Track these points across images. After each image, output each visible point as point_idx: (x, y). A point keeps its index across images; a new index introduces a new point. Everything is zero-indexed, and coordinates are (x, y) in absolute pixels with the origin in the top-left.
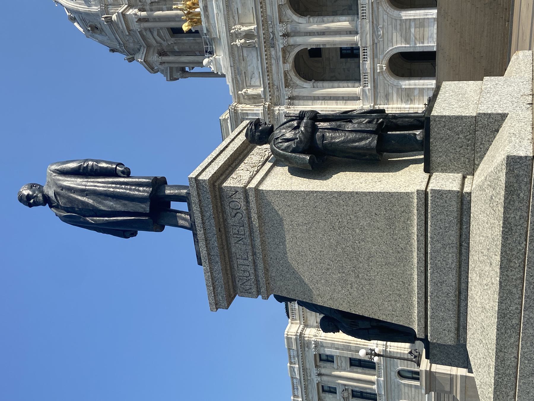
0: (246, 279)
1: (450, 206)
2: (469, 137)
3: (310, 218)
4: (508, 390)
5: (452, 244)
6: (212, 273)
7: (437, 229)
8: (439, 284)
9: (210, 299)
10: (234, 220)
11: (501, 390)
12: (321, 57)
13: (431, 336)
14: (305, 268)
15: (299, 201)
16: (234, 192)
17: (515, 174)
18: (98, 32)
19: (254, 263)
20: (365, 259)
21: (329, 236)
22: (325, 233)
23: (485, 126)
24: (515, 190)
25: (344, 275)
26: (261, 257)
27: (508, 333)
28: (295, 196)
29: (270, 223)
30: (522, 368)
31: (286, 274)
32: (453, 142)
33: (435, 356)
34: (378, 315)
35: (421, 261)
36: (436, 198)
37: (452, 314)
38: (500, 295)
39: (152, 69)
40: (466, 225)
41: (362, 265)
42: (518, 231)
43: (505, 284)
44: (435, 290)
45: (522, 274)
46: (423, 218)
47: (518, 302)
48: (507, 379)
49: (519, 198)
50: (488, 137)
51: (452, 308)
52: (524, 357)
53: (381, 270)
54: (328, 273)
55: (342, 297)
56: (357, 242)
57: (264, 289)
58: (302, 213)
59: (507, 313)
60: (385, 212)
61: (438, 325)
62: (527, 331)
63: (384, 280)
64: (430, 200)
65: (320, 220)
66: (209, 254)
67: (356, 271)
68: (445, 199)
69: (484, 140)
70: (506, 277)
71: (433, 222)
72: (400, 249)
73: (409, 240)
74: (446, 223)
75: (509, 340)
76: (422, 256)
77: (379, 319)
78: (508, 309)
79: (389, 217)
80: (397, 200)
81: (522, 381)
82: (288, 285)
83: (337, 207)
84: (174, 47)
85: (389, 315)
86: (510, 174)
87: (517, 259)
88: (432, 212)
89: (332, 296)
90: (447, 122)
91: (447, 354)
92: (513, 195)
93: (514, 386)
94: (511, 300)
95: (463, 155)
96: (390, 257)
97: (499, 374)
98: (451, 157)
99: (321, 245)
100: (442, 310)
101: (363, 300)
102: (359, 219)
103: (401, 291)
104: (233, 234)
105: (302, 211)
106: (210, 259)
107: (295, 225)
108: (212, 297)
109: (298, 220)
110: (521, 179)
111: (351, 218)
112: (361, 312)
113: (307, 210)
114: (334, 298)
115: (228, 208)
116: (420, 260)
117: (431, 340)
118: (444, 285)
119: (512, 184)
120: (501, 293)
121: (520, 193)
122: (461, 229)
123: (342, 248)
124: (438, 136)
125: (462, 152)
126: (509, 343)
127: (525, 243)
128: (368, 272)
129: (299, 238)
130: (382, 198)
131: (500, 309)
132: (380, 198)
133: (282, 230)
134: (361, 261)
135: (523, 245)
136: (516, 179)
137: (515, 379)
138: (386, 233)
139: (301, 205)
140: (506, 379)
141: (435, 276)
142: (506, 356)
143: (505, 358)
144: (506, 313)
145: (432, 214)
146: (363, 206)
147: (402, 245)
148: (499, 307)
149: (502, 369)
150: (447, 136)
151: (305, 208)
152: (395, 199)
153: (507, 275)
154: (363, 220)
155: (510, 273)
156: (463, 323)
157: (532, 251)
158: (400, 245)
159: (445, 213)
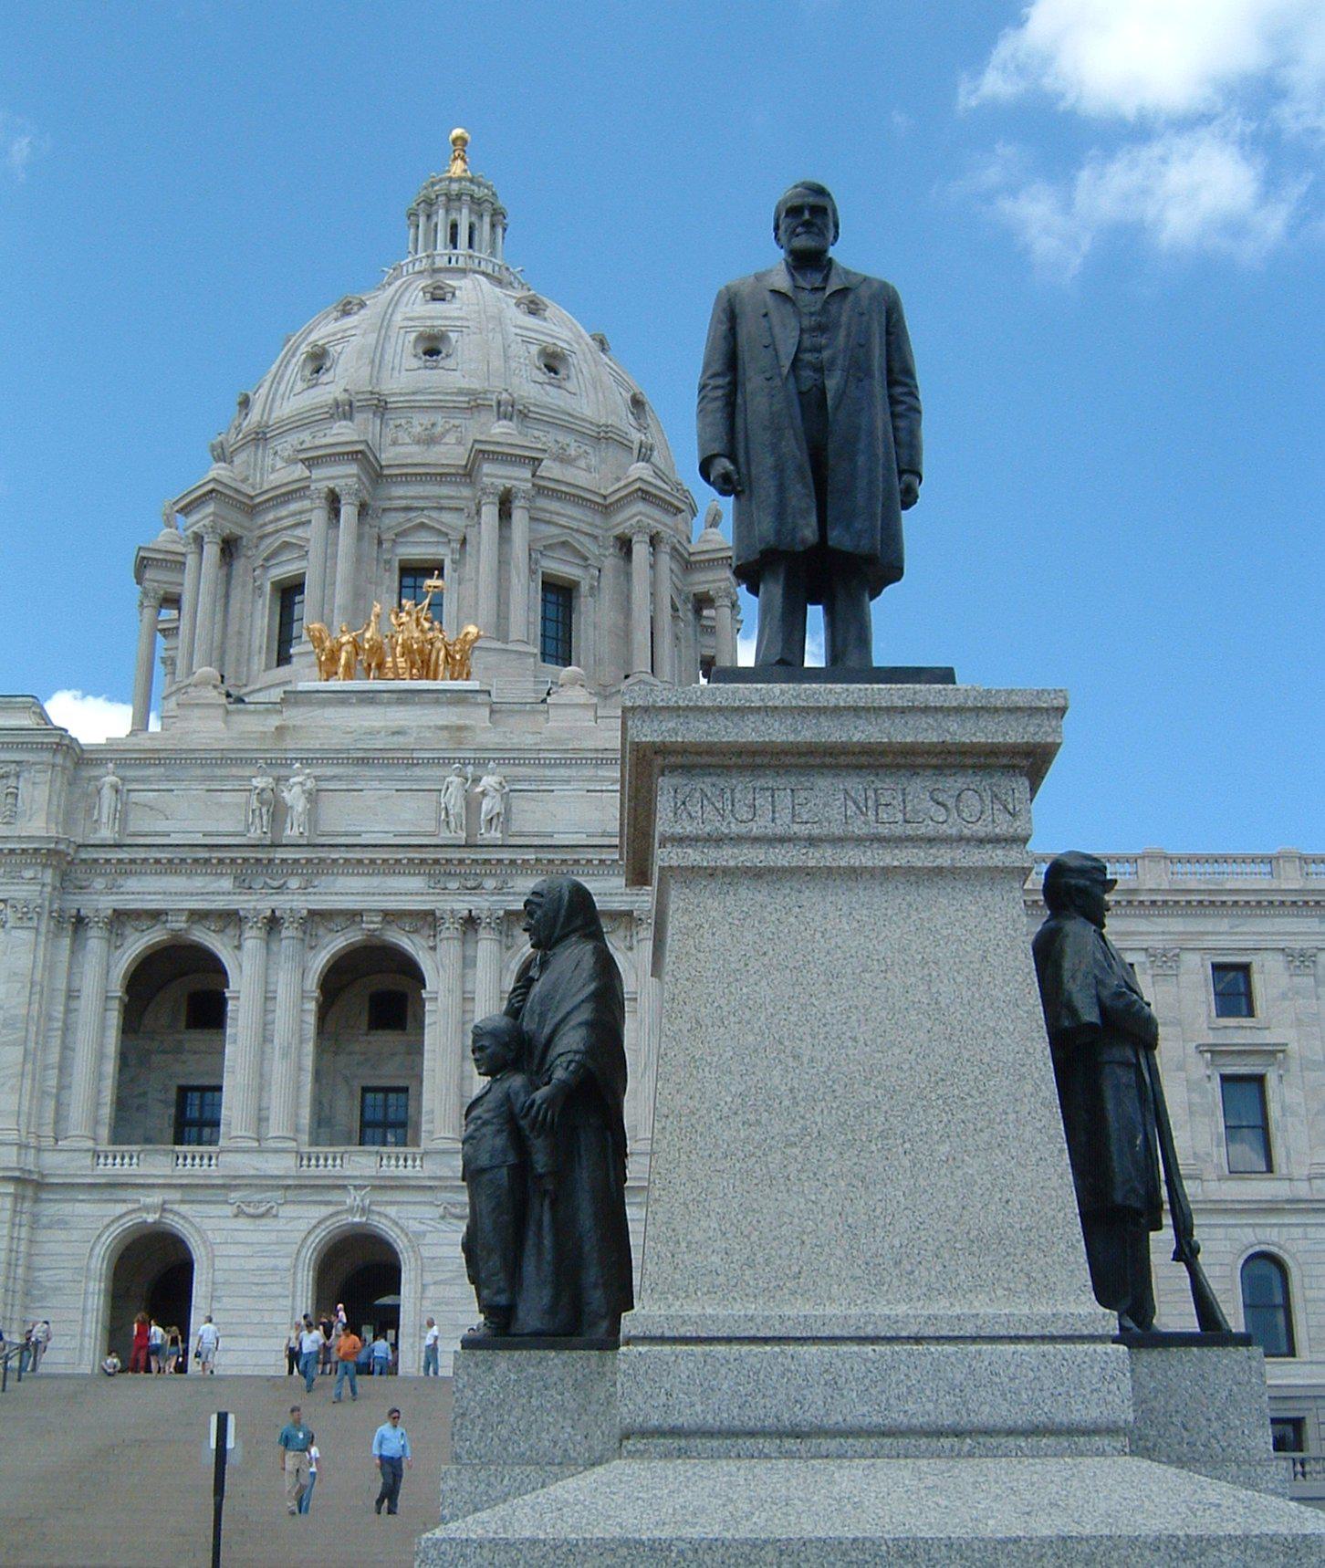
5: (968, 1409)
10: (922, 797)
12: (189, 1026)
13: (640, 1353)
16: (1010, 807)
18: (307, 373)
19: (782, 840)
20: (856, 1167)
21: (911, 1068)
22: (918, 1056)
25: (786, 1103)
31: (755, 931)
32: (1195, 1405)
35: (894, 1326)
36: (1103, 1365)
37: (729, 1416)
41: (833, 1157)
43: (1015, 1554)
44: (806, 1366)
51: (752, 1415)
54: (782, 1056)
56: (907, 1145)
58: (970, 993)
59: (917, 1563)
65: (957, 1045)
67: (808, 1138)
70: (1035, 1555)
71: (1027, 1359)
74: (1030, 1393)
76: (912, 1330)
79: (1003, 1236)
82: (713, 934)
83: (1008, 1095)
88: (1059, 1357)
90: (1248, 1388)
92: (1286, 1555)
95: (1162, 1432)
98: (1155, 1404)
99: (873, 1041)
100: (741, 1388)
101: (710, 1156)
102: (982, 1154)
103: (767, 1269)
104: (876, 790)
107: (926, 971)
109: (946, 981)
113: (983, 1010)
116: (896, 1322)
117: (624, 1354)
118: (830, 1391)
122: (1011, 1432)
128: (812, 1176)
132: (1061, 1215)
134: (846, 1156)
138: (954, 1228)
139: (993, 992)
141: (856, 1367)
145: (1055, 1356)
146: (1025, 1167)
147: (925, 1273)
148: (936, 1541)
149: (718, 1558)
150: (1212, 1391)
152: (1066, 1255)
153: (1042, 1556)
154: (983, 1167)
159: (1060, 1389)
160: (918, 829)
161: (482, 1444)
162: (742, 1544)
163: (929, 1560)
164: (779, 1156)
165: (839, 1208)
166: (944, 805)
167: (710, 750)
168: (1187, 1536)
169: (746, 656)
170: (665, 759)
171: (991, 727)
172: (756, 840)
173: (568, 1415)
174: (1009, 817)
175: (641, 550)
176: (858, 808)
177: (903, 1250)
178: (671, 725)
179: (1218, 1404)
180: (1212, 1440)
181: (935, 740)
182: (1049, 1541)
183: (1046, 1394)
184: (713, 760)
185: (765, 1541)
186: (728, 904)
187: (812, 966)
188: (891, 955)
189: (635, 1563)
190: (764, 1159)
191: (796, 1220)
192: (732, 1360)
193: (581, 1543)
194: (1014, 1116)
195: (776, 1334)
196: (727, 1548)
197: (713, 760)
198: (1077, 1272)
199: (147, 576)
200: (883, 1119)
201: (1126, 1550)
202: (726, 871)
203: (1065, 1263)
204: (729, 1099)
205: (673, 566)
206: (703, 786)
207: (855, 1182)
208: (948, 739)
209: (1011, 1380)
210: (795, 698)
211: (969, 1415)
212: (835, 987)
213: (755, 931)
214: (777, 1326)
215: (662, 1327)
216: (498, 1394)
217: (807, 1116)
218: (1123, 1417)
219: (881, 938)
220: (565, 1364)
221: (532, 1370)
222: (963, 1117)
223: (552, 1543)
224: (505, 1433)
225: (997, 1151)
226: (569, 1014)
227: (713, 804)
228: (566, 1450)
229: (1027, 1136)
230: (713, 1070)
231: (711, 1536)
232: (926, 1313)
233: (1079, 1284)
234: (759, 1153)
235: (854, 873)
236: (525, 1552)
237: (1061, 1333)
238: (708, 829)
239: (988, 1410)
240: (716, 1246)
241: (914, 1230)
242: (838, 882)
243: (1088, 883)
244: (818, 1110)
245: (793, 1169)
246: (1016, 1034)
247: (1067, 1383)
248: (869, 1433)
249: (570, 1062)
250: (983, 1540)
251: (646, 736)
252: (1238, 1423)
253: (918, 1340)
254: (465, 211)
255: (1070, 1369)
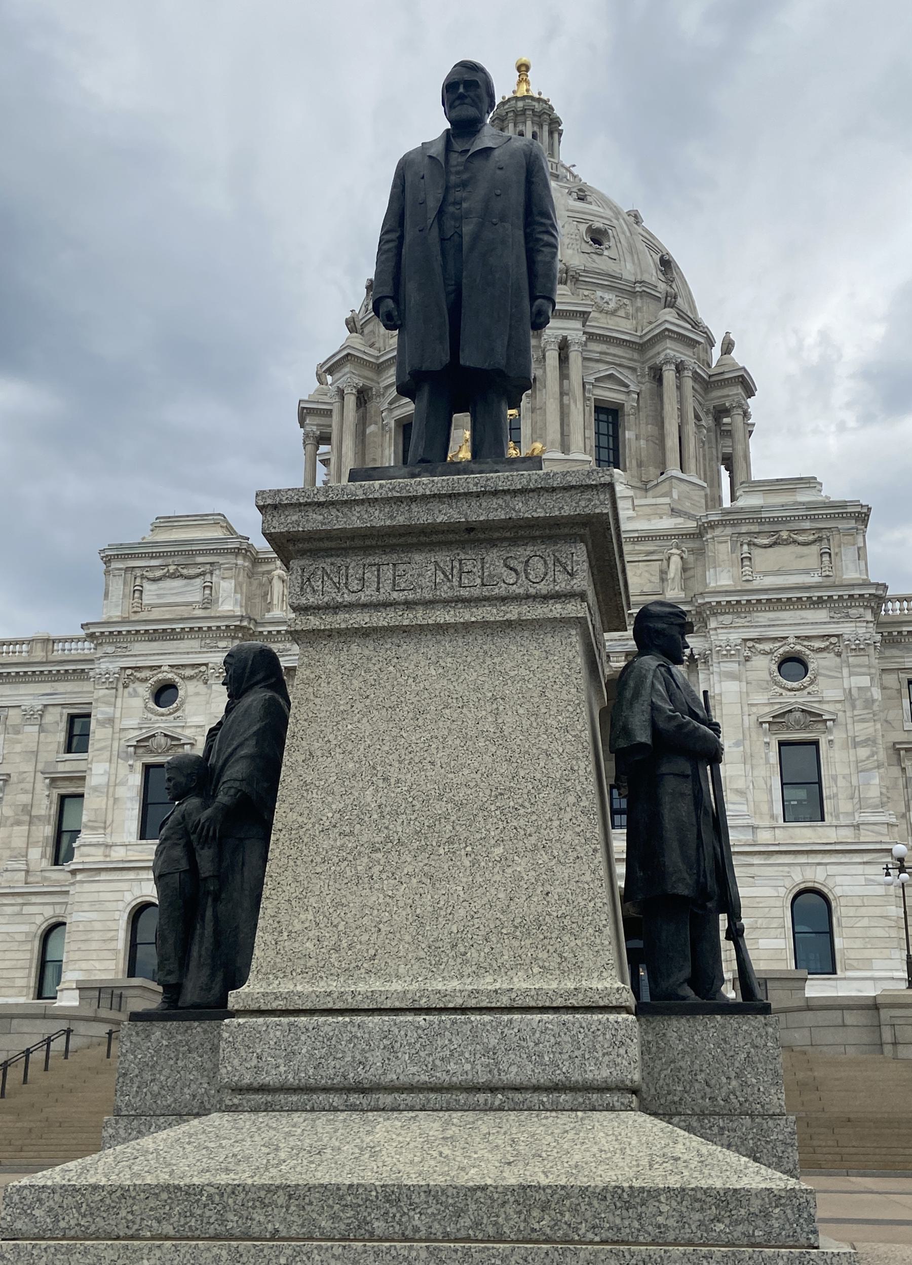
0: (339, 583)
1: (596, 1064)
2: (735, 1101)
3: (518, 740)
4: (175, 1219)
5: (499, 1069)
6: (362, 502)
7: (534, 1034)
8: (385, 1042)
9: (290, 492)
10: (497, 564)
11: (176, 1202)
13: (239, 1025)
14: (383, 727)
15: (560, 718)
16: (569, 568)
17: (770, 1209)
19: (386, 605)
21: (477, 785)
23: (764, 1137)
24: (731, 1211)
25: (375, 816)
26: (406, 623)
27: (342, 1211)
28: (571, 709)
29: (493, 647)
30: (262, 1250)
31: (361, 679)
32: (717, 1065)
33: (143, 1036)
34: (275, 897)
36: (613, 1032)
37: (308, 1075)
38: (451, 1188)
39: (330, 371)
40: (548, 1101)
41: (409, 860)
42: (627, 1223)
43: (482, 1200)
44: (369, 1033)
45: (513, 1236)
46: (559, 1002)
47: (433, 1231)
48: (210, 1217)
49: (712, 1220)
50: (739, 1143)
51: (324, 1074)
52: (295, 1254)
53: (401, 904)
55: (314, 811)
56: (469, 849)
57: (317, 623)
58: (529, 722)
59: (401, 1206)
60: (555, 914)
61: (272, 1043)
62: (372, 1258)
63: (375, 912)
64: (608, 1019)
65: (515, 765)
66: (413, 499)
67: (390, 844)
68: (614, 1053)
69: (732, 1134)
70: (500, 1201)
72: (462, 950)
73: (491, 971)
74: (551, 1056)
75: (323, 1216)
76: (458, 1002)
77: (263, 900)
78: (414, 1210)
79: (543, 923)
80: (589, 942)
81: (224, 1253)
82: (329, 683)
83: (554, 805)
84: (376, 423)
85: (279, 922)
86: (770, 1199)
87: (553, 1223)
88: (577, 1025)
89: (313, 786)
90: (764, 1052)
91: (153, 1066)
93: (189, 1234)
94: (439, 1214)
96: (440, 926)
97: (222, 1195)
98: (681, 1063)
99: (448, 764)
101: (312, 861)
102: (529, 854)
103: (350, 953)
104: (460, 561)
105: (535, 724)
106: (399, 500)
107: (495, 706)
108: (296, 497)
109: (510, 713)
110: (760, 1222)
111: (530, 835)
112: (277, 855)
113: (539, 736)
114: (307, 790)
115: (528, 553)
116: (445, 996)
117: (226, 1025)
118: (387, 1054)
119: (744, 1203)
120: (455, 1190)
121: (723, 1223)
122: (537, 1089)
123: (449, 814)
124: (729, 1033)
125: (697, 1086)
126: (315, 1215)
127: (597, 1239)
128: (390, 875)
129: (462, 713)
130: (590, 909)
131: (409, 1189)
132: (592, 904)
133: (478, 676)
134: (419, 859)
135: (590, 1236)
136: (757, 1212)
137: (212, 1235)
138: (502, 917)
139: (549, 721)
140: (208, 1213)
141: (409, 1034)
142: (275, 1210)
143: (270, 1208)
144: (402, 1204)
145: (573, 1024)
147: (475, 955)
148: (417, 1188)
149: (239, 1202)
150: (732, 1053)
151: (543, 729)
152: (593, 938)
155: (510, 1209)
156: (283, 1101)
157: (592, 1258)
158: (473, 950)
159: (577, 1053)
160: (492, 590)
161: (138, 1099)
162: (259, 1189)
163: (411, 1204)
164: (365, 860)
165: (410, 901)
166: (515, 571)
167: (328, 535)
168: (631, 1187)
169: (465, 454)
170: (294, 545)
171: (551, 504)
172: (364, 606)
173: (205, 1073)
174: (567, 577)
175: (669, 375)
176: (446, 576)
177: (459, 935)
178: (295, 518)
179: (737, 1064)
180: (732, 1097)
181: (503, 517)
182: (511, 1189)
183: (565, 1057)
184: (332, 544)
185: (278, 1187)
186: (342, 658)
187: (403, 705)
188: (467, 694)
189: (173, 1205)
190: (353, 862)
191: (375, 912)
192: (311, 1029)
193: (131, 1188)
194: (558, 822)
195: (348, 1007)
196: (247, 1194)
197: (332, 544)
198: (601, 952)
199: (308, 421)
200: (451, 828)
201: (577, 1198)
202: (340, 632)
203: (591, 945)
204: (330, 815)
205: (697, 387)
206: (324, 565)
207: (424, 880)
208: (514, 515)
209: (536, 1044)
210: (390, 490)
211: (500, 1075)
212: (420, 722)
213: (361, 679)
214: (350, 1000)
215: (259, 1002)
216: (152, 1057)
217: (390, 827)
218: (629, 1077)
219: (461, 680)
220: (205, 1031)
221: (179, 1037)
222: (516, 824)
223: (109, 1188)
224: (156, 1088)
225: (543, 853)
226: (235, 749)
227: (331, 579)
228: (202, 1103)
229: (568, 838)
230: (319, 793)
231: (236, 1182)
232: (470, 988)
233: (603, 962)
234: (350, 858)
235: (441, 629)
236: (87, 1196)
237: (581, 1004)
238: (326, 600)
239: (516, 1070)
240: (311, 934)
241: (469, 918)
242: (429, 637)
243: (665, 626)
244: (400, 821)
245: (376, 870)
246: (564, 755)
247: (583, 1047)
248: (411, 1089)
249: (230, 788)
250: (456, 1188)
251: (274, 528)
252: (754, 1081)
253: (463, 1010)
254: (529, 123)
255: (586, 1036)
